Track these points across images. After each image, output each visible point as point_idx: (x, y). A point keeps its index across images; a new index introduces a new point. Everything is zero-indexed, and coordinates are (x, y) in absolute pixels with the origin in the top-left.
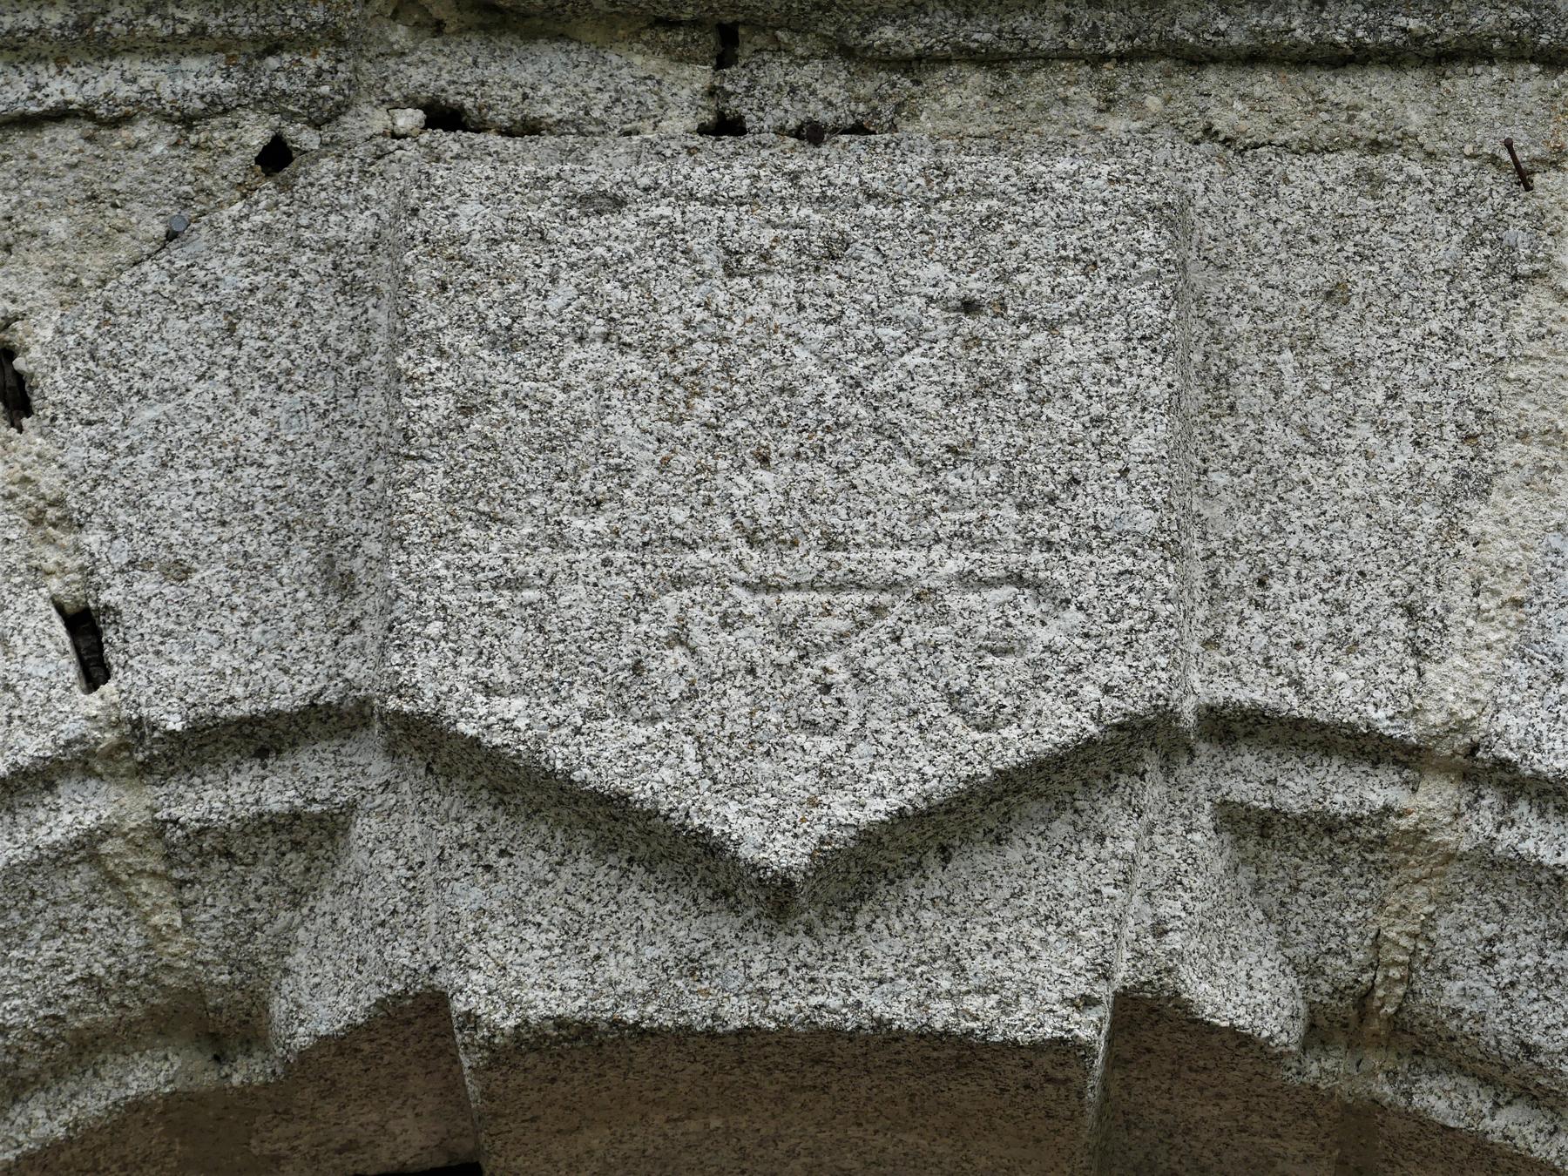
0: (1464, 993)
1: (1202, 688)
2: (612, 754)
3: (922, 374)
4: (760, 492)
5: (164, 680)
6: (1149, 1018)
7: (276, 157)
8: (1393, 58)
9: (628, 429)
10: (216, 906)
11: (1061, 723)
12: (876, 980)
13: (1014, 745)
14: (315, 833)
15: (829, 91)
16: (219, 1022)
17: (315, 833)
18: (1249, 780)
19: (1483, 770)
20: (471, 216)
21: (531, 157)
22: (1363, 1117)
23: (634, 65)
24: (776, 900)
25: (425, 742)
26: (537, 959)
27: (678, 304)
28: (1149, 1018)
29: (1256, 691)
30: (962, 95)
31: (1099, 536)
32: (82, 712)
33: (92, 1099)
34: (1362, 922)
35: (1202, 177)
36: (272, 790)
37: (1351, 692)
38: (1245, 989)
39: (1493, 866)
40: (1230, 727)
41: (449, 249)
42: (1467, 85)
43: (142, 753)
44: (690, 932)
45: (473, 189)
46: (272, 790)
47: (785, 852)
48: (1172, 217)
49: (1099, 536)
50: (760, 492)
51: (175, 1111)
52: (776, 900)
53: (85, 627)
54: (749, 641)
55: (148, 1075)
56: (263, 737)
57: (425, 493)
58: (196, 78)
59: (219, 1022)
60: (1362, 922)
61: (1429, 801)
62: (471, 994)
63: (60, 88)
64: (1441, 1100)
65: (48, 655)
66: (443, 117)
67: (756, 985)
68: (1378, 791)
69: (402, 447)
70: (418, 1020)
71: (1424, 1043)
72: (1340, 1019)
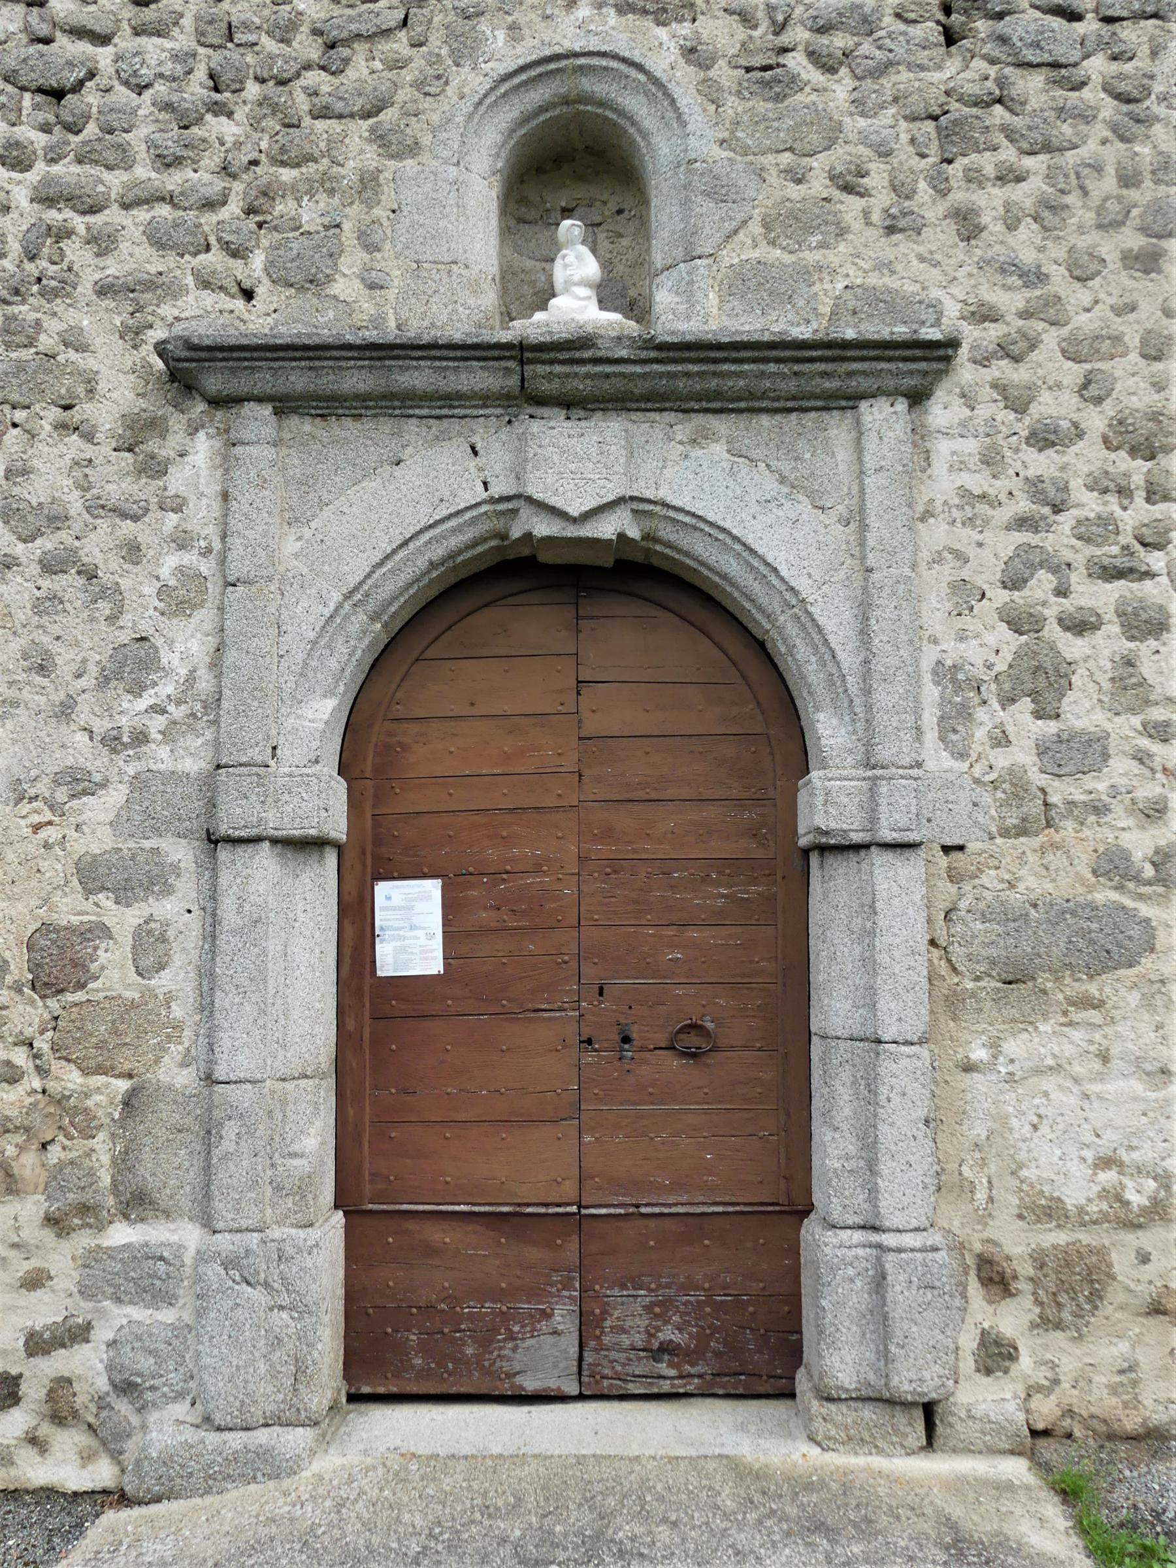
0: (662, 534)
1: (629, 493)
2: (553, 501)
3: (594, 451)
4: (572, 467)
5: (496, 490)
6: (622, 536)
7: (510, 422)
8: (655, 410)
9: (556, 458)
10: (502, 521)
11: (611, 498)
12: (588, 531)
13: (605, 500)
14: (515, 512)
15: (582, 414)
16: (503, 536)
17: (515, 512)
18: (635, 506)
19: (729, 533)
20: (535, 430)
21: (543, 422)
22: (649, 549)
23: (556, 410)
24: (574, 520)
25: (530, 500)
26: (543, 528)
27: (562, 441)
28: (622, 536)
29: (636, 494)
30: (599, 414)
31: (616, 473)
32: (485, 495)
33: (487, 546)
34: (648, 524)
35: (630, 426)
36: (510, 506)
37: (649, 494)
38: (634, 533)
39: (666, 517)
40: (632, 498)
41: (532, 434)
42: (665, 414)
43: (493, 501)
44: (564, 524)
45: (535, 426)
46: (510, 506)
47: (575, 514)
48: (626, 431)
49: (616, 473)
50: (572, 467)
51: (498, 548)
52: (574, 520)
53: (485, 483)
54: (571, 486)
55: (493, 543)
56: (508, 499)
57: (529, 466)
58: (499, 411)
59: (503, 536)
60: (648, 524)
61: (658, 508)
62: (535, 532)
63: (481, 412)
64: (658, 548)
65: (481, 487)
66: (531, 417)
67: (572, 531)
68: (651, 507)
69: (526, 460)
70: (528, 536)
71: (656, 540)
72: (646, 537)
